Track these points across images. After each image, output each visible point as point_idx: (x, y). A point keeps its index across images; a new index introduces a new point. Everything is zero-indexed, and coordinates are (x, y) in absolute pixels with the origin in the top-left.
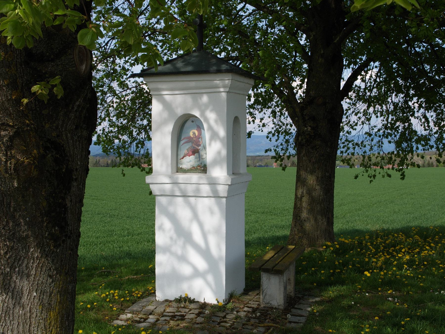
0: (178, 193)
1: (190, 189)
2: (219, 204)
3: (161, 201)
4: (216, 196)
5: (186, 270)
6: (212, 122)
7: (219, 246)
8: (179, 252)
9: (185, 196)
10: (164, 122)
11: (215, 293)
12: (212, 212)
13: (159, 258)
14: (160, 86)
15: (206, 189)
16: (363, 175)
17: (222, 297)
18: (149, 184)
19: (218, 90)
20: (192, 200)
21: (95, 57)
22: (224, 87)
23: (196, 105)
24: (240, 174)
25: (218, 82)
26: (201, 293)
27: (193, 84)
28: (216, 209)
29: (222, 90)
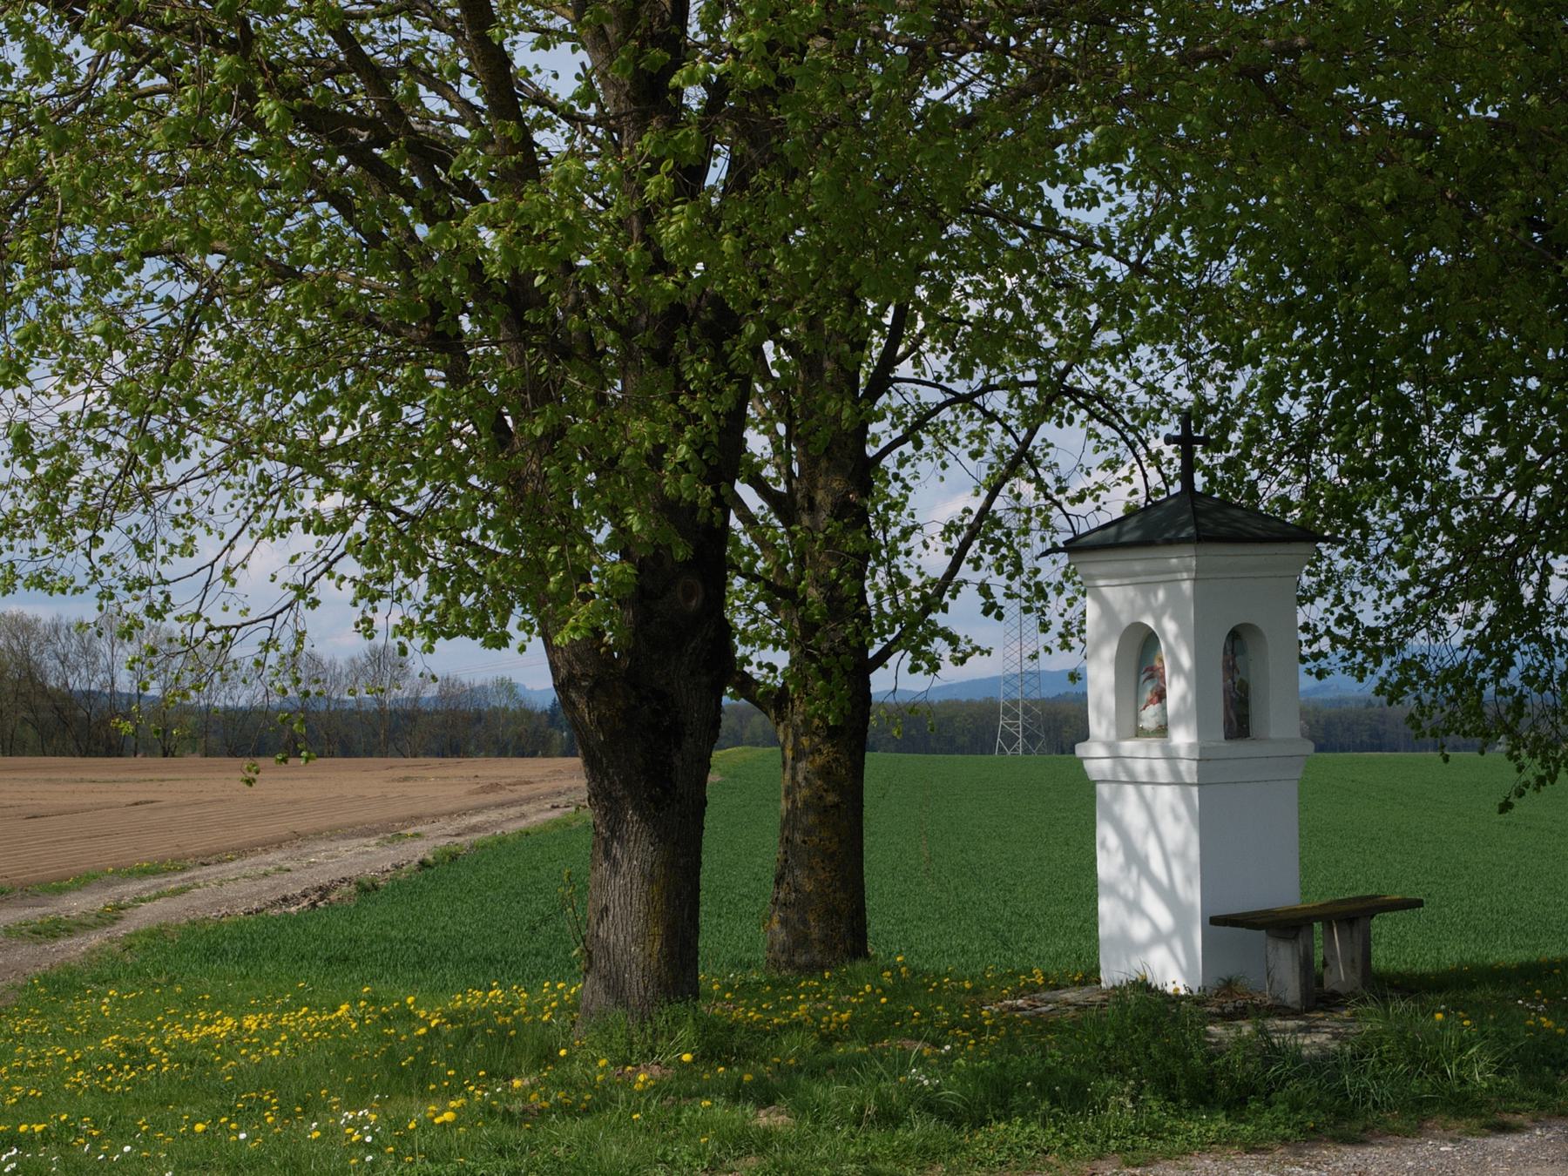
0: (1124, 778)
1: (1140, 767)
2: (1187, 799)
3: (1104, 790)
4: (1178, 781)
5: (1140, 930)
6: (1171, 638)
7: (1188, 880)
8: (1131, 894)
9: (1136, 783)
10: (1102, 640)
11: (1186, 974)
12: (1177, 818)
13: (1105, 906)
14: (1094, 569)
15: (1161, 767)
16: (556, 76)
17: (1196, 985)
18: (1081, 760)
19: (1179, 576)
20: (1147, 789)
21: (12, 1094)
22: (1188, 570)
23: (1148, 608)
24: (1335, 995)
25: (1174, 561)
26: (1163, 973)
27: (1138, 566)
28: (1182, 810)
29: (1185, 575)
